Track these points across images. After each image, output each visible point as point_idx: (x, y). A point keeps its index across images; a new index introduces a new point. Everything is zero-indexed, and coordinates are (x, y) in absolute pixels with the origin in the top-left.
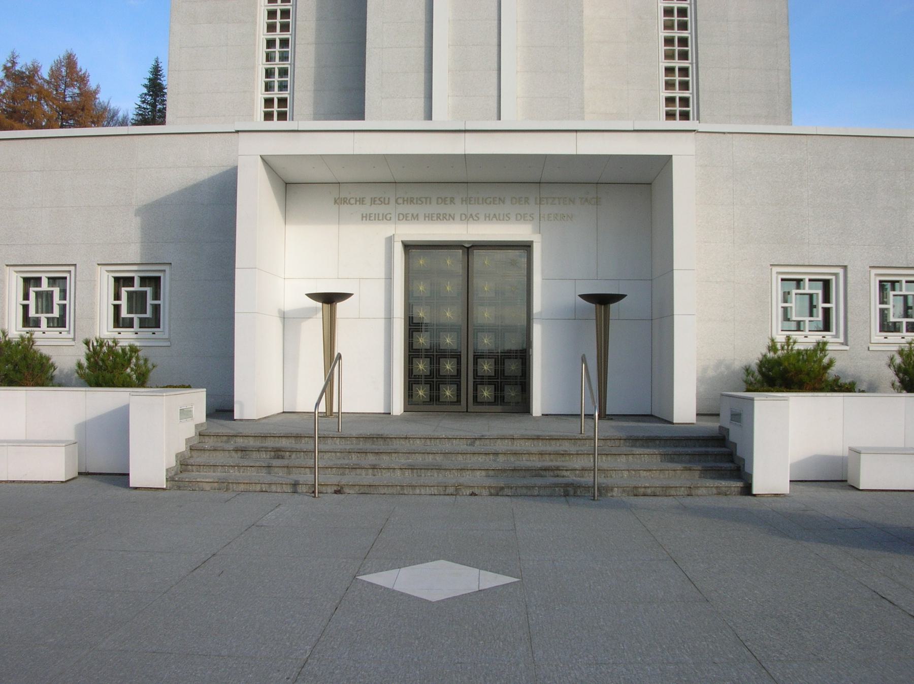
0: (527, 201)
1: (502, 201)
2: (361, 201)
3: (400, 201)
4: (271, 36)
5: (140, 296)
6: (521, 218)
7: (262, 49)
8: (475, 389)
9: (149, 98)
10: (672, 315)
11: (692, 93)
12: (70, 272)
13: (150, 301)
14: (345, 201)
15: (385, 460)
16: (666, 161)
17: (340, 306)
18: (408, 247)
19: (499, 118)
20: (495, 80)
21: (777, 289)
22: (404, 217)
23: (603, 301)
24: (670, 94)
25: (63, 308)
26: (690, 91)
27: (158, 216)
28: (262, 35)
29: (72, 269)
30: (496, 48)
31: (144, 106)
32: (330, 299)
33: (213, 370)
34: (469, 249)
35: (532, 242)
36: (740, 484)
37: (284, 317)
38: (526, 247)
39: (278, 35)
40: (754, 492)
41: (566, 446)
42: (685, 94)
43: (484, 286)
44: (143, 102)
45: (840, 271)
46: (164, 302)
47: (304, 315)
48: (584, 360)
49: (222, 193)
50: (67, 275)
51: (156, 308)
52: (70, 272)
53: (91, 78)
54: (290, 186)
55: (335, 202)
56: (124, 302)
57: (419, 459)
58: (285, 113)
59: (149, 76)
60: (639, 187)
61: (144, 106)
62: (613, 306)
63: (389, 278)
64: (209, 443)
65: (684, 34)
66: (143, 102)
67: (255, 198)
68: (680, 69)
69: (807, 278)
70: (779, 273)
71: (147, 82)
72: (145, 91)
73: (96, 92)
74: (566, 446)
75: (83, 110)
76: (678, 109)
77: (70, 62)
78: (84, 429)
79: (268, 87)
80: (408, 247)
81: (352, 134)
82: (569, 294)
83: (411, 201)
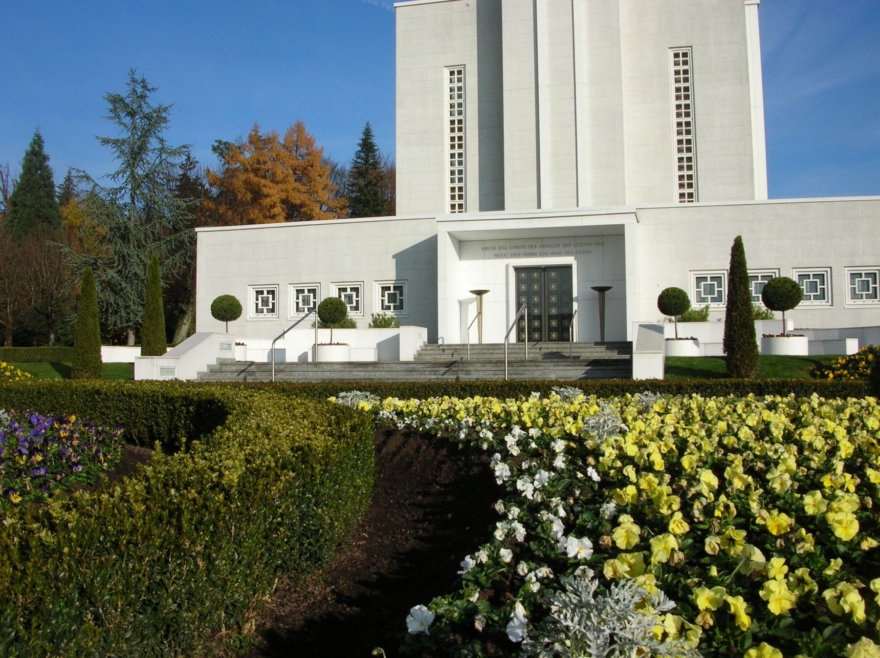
2: (494, 248)
4: (453, 152)
5: (395, 295)
6: (568, 254)
7: (448, 159)
8: (549, 334)
9: (363, 155)
13: (398, 297)
14: (487, 248)
17: (484, 296)
18: (518, 269)
19: (539, 207)
23: (602, 290)
24: (681, 173)
25: (357, 302)
27: (402, 258)
28: (448, 151)
31: (359, 161)
32: (480, 293)
33: (429, 320)
37: (460, 303)
38: (569, 267)
39: (457, 151)
44: (358, 158)
45: (829, 270)
46: (405, 298)
47: (470, 301)
49: (430, 247)
51: (401, 301)
53: (316, 141)
54: (461, 244)
56: (386, 298)
59: (362, 136)
61: (359, 161)
64: (428, 348)
66: (358, 158)
67: (446, 251)
68: (687, 158)
71: (360, 142)
72: (360, 149)
73: (321, 152)
75: (312, 166)
76: (686, 182)
77: (299, 129)
78: (380, 346)
79: (452, 181)
80: (518, 269)
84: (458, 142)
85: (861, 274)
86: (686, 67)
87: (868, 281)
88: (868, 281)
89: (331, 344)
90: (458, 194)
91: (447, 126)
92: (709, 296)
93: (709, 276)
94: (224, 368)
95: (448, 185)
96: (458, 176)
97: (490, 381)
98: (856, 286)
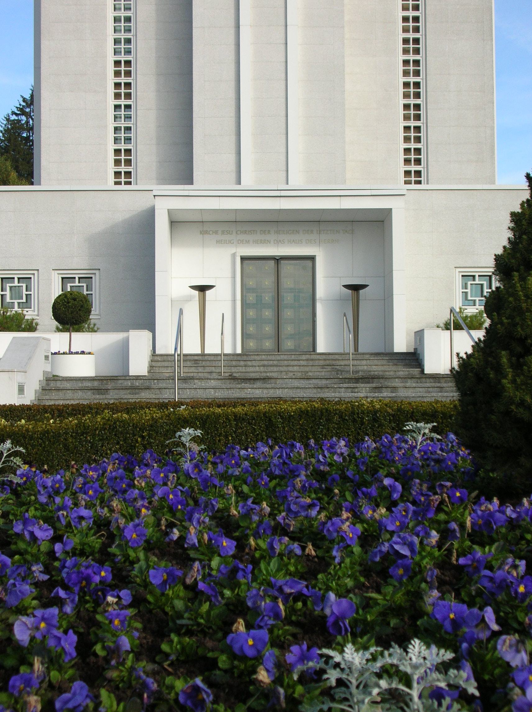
0: (312, 232)
1: (298, 232)
2: (216, 232)
3: (239, 232)
6: (309, 242)
10: (393, 295)
11: (423, 145)
12: (34, 274)
15: (249, 363)
16: (390, 211)
17: (208, 293)
18: (243, 259)
19: (239, 182)
20: (284, 141)
21: (459, 281)
22: (241, 242)
23: (356, 288)
24: (407, 146)
26: (422, 144)
28: (111, 102)
29: (36, 272)
30: (285, 118)
32: (202, 289)
34: (278, 260)
35: (315, 256)
36: (420, 370)
38: (312, 259)
40: (425, 373)
41: (337, 357)
42: (418, 146)
43: (287, 283)
47: (189, 299)
48: (345, 315)
50: (92, 276)
52: (34, 274)
55: (201, 233)
57: (266, 363)
58: (130, 160)
60: (376, 225)
62: (361, 292)
63: (234, 277)
65: (418, 101)
69: (477, 274)
70: (459, 272)
74: (337, 357)
76: (413, 157)
80: (243, 259)
81: (218, 198)
82: (337, 288)
83: (245, 232)
84: (123, 90)
85: (474, 277)
86: (416, 14)
87: (482, 285)
88: (482, 285)
89: (71, 353)
90: (124, 157)
91: (111, 69)
92: (16, 302)
93: (16, 277)
94: (52, 384)
95: (111, 147)
96: (123, 133)
97: (339, 403)
98: (468, 291)
